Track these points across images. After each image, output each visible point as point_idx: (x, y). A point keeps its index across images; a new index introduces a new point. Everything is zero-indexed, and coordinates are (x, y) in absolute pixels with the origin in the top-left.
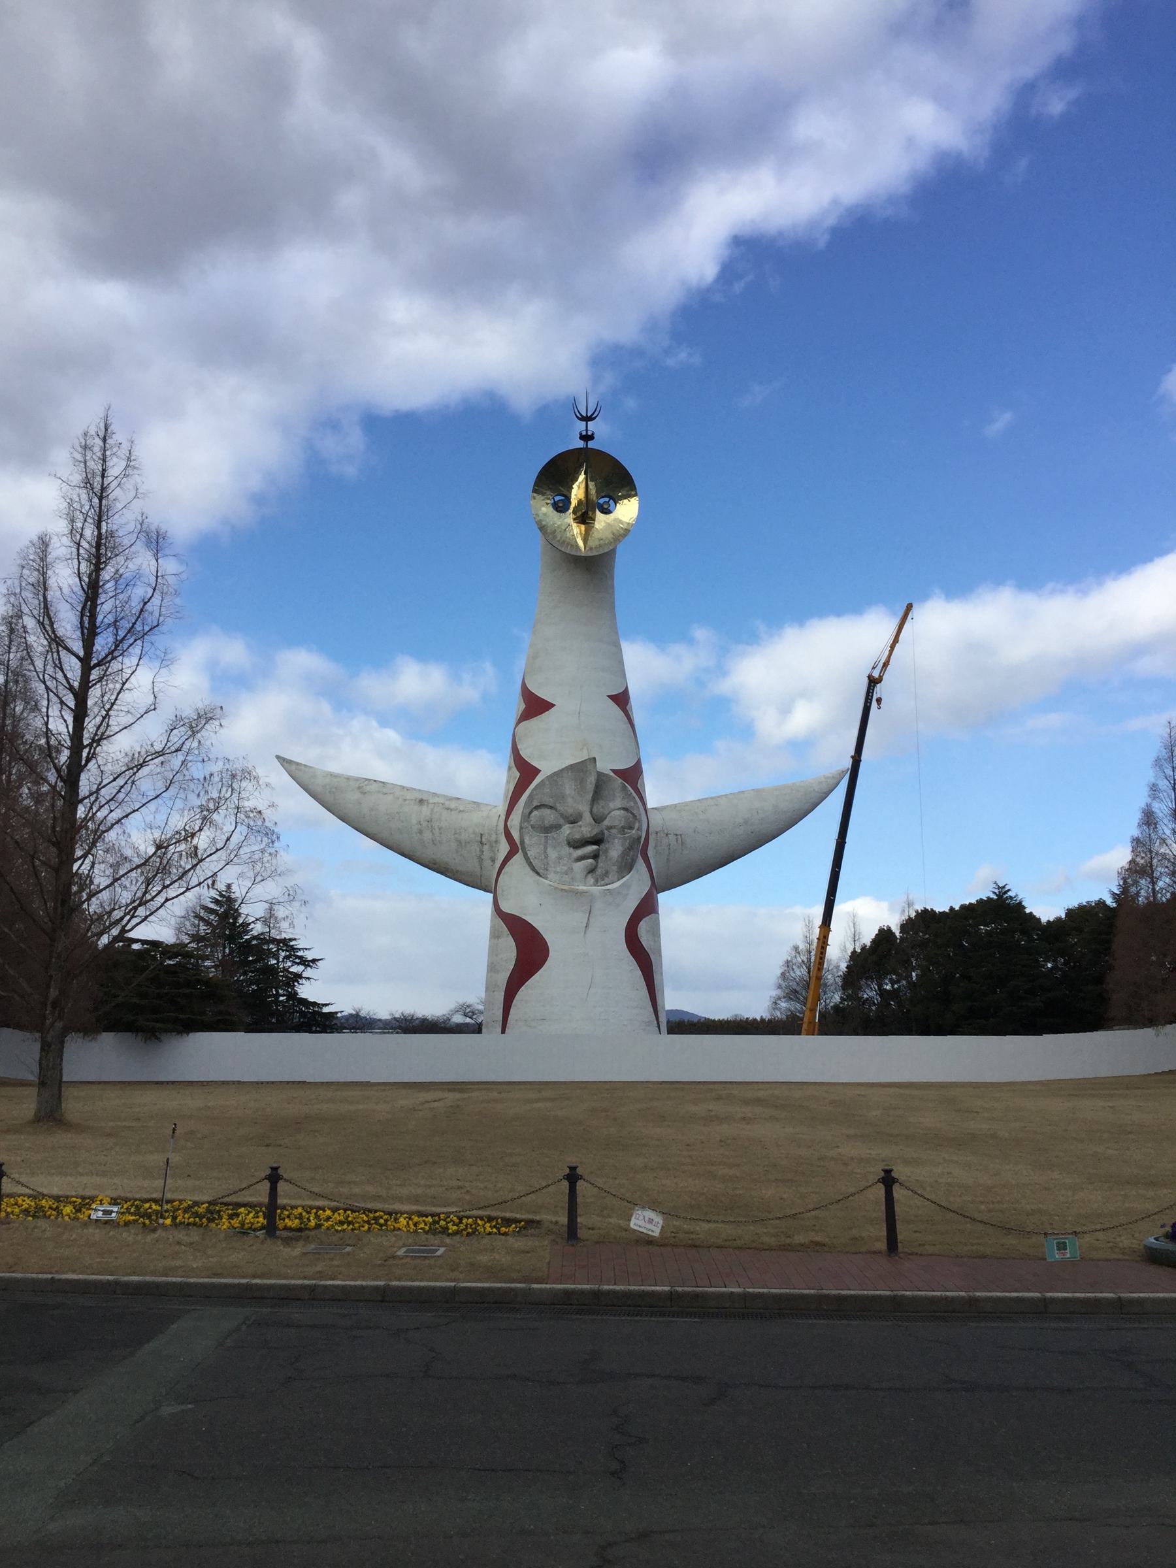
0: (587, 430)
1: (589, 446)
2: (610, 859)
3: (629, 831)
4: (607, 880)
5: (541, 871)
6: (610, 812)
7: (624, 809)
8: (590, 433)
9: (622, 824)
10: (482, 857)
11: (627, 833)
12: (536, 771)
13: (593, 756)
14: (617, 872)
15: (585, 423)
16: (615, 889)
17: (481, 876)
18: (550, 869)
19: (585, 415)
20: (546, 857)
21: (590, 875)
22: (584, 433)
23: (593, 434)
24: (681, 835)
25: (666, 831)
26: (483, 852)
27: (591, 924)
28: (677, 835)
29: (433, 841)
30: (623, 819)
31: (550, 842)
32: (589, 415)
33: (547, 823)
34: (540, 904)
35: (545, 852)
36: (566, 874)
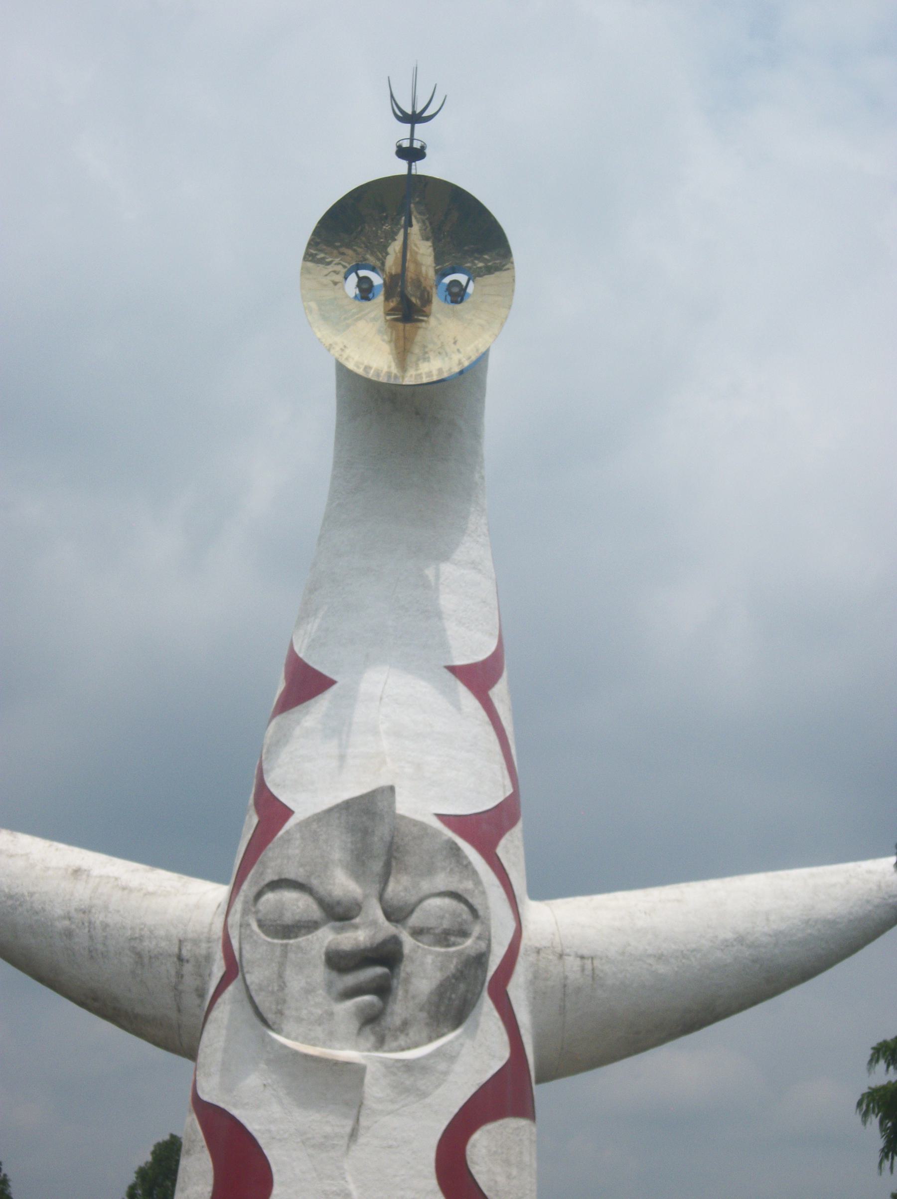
0: (412, 139)
1: (413, 172)
2: (414, 997)
3: (459, 940)
4: (402, 1040)
5: (270, 1016)
6: (421, 901)
7: (455, 895)
8: (417, 145)
9: (445, 926)
10: (180, 988)
11: (454, 944)
12: (287, 813)
13: (390, 783)
14: (427, 1024)
15: (409, 126)
16: (419, 1059)
17: (179, 1027)
18: (287, 1012)
19: (409, 111)
20: (282, 987)
21: (367, 1029)
22: (406, 144)
23: (423, 148)
24: (592, 958)
25: (559, 950)
26: (182, 976)
27: (361, 1131)
28: (582, 957)
29: (90, 951)
30: (447, 915)
31: (291, 956)
32: (418, 110)
33: (288, 918)
34: (265, 1085)
35: (280, 976)
36: (320, 1025)
